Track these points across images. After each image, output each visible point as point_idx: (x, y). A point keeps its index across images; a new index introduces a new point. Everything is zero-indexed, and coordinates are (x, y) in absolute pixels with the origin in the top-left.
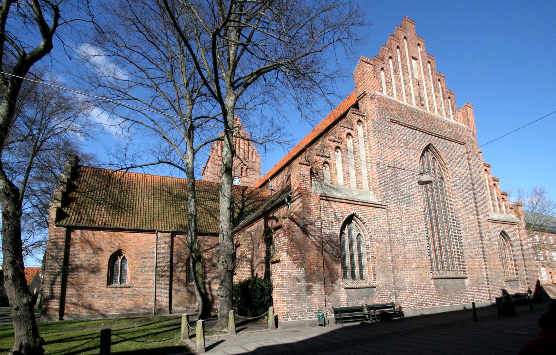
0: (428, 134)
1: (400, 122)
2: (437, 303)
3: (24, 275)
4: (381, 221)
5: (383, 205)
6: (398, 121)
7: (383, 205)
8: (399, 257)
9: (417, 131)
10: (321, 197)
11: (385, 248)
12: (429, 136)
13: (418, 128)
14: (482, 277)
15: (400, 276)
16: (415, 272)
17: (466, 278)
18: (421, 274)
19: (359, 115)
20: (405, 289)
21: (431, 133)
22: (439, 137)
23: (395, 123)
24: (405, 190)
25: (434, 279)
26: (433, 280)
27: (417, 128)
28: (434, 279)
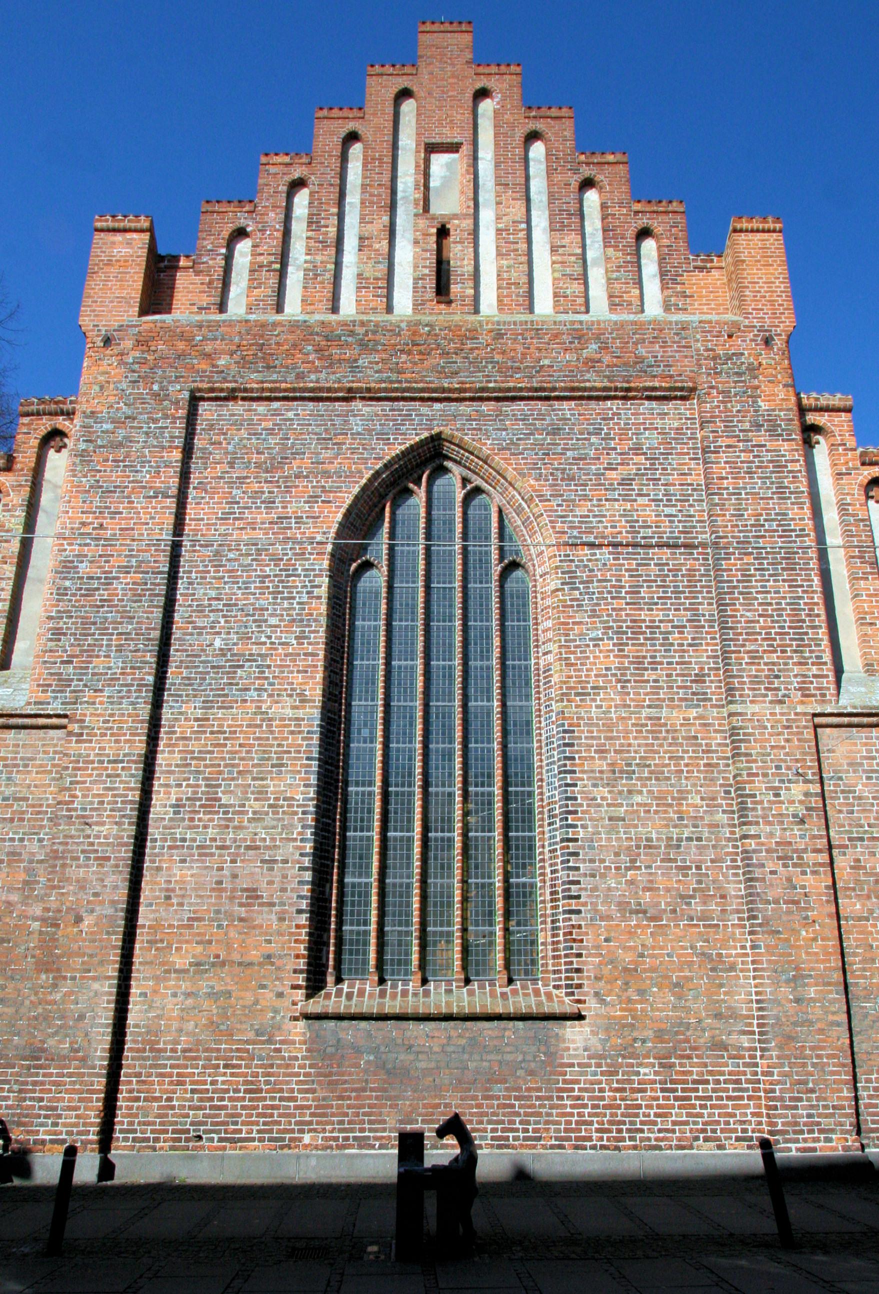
0: (422, 399)
1: (246, 390)
2: (307, 1138)
3: (108, 1074)
4: (32, 777)
5: (49, 716)
6: (234, 390)
7: (49, 716)
8: (79, 920)
9: (357, 405)
10: (818, 720)
11: (26, 883)
12: (437, 406)
13: (359, 390)
14: (718, 1016)
15: (63, 1003)
16: (185, 986)
17: (579, 1017)
18: (229, 994)
19: (56, 414)
20: (83, 1059)
21: (444, 390)
22: (497, 399)
23: (226, 399)
24: (218, 643)
25: (307, 1017)
26: (302, 1024)
27: (350, 390)
28: (307, 1017)
